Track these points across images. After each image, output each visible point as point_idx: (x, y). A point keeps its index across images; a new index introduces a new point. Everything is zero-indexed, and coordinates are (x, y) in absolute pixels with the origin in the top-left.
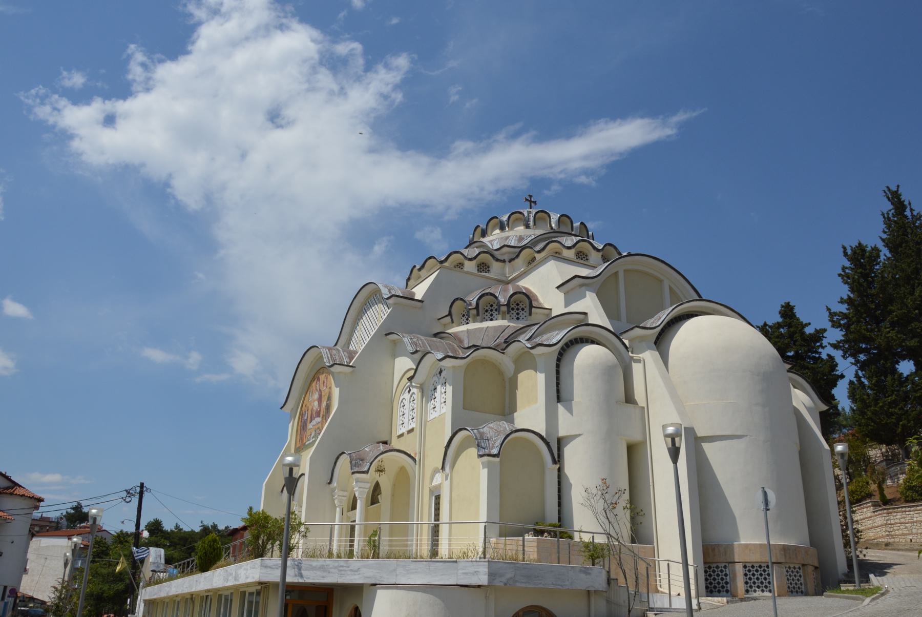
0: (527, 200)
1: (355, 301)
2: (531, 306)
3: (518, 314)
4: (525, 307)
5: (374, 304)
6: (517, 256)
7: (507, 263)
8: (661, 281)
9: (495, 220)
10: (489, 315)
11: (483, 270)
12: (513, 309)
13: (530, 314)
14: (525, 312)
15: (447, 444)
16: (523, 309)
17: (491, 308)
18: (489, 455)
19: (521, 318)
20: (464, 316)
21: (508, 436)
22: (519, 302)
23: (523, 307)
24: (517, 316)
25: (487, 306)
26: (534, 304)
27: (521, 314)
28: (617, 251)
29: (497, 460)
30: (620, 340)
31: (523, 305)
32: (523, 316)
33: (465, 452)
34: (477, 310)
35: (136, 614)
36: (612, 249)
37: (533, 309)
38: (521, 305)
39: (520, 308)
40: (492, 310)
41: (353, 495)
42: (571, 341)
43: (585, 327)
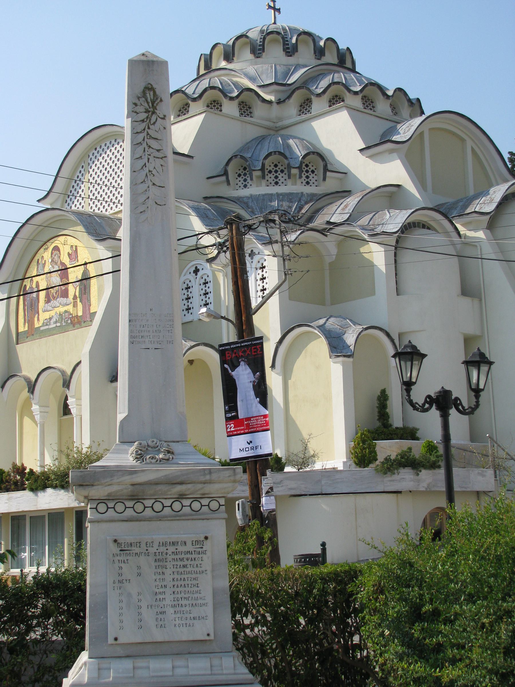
0: (270, 7)
1: (79, 143)
2: (326, 169)
3: (276, 177)
4: (315, 169)
5: (105, 150)
6: (289, 97)
7: (275, 105)
8: (463, 140)
9: (243, 40)
10: (273, 177)
11: (248, 115)
12: (270, 172)
13: (324, 179)
14: (316, 175)
15: (280, 340)
16: (282, 171)
17: (275, 169)
18: (344, 356)
19: (280, 182)
20: (239, 175)
21: (360, 334)
22: (308, 163)
23: (282, 168)
24: (307, 180)
25: (270, 166)
26: (329, 167)
27: (311, 177)
28: (406, 97)
29: (351, 360)
30: (453, 224)
31: (312, 166)
32: (282, 180)
33: (303, 352)
34: (262, 173)
35: (272, 485)
36: (375, 88)
37: (328, 174)
38: (310, 166)
39: (310, 170)
40: (276, 172)
41: (65, 396)
42: (414, 223)
43: (325, 197)
